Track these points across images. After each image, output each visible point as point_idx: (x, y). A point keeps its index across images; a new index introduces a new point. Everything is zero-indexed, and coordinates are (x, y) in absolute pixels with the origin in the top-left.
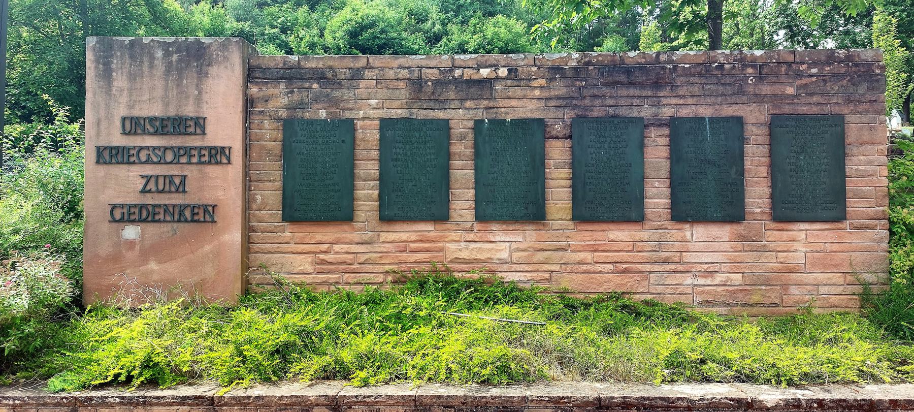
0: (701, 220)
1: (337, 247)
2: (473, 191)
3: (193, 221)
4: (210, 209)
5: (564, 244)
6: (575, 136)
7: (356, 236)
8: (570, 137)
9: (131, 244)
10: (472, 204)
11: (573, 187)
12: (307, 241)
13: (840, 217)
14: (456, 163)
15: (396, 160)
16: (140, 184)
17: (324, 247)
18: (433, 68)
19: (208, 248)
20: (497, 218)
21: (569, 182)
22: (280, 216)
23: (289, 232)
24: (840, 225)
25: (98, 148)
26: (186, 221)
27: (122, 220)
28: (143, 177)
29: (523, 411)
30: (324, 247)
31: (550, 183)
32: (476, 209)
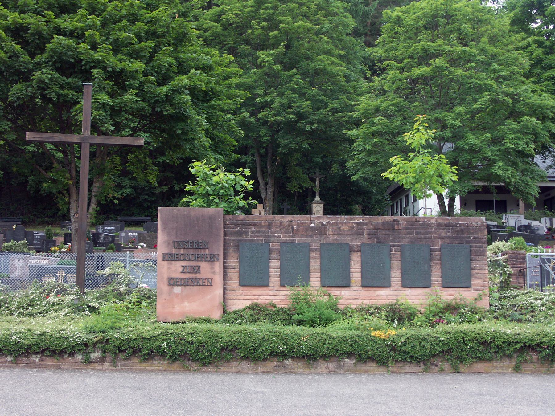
0: (189, 283)
1: (261, 297)
2: (319, 274)
3: (203, 285)
4: (210, 280)
5: (358, 296)
6: (362, 250)
7: (271, 292)
8: (360, 251)
9: (177, 295)
10: (319, 279)
11: (362, 272)
12: (249, 294)
13: (468, 287)
14: (312, 261)
15: (287, 260)
16: (181, 269)
17: (256, 297)
18: (178, 323)
19: (209, 297)
20: (189, 283)
21: (360, 270)
22: (238, 284)
23: (241, 290)
24: (468, 289)
25: (163, 254)
26: (200, 285)
27: (173, 285)
28: (182, 266)
29: (1, 127)
30: (256, 297)
31: (352, 270)
32: (321, 281)
